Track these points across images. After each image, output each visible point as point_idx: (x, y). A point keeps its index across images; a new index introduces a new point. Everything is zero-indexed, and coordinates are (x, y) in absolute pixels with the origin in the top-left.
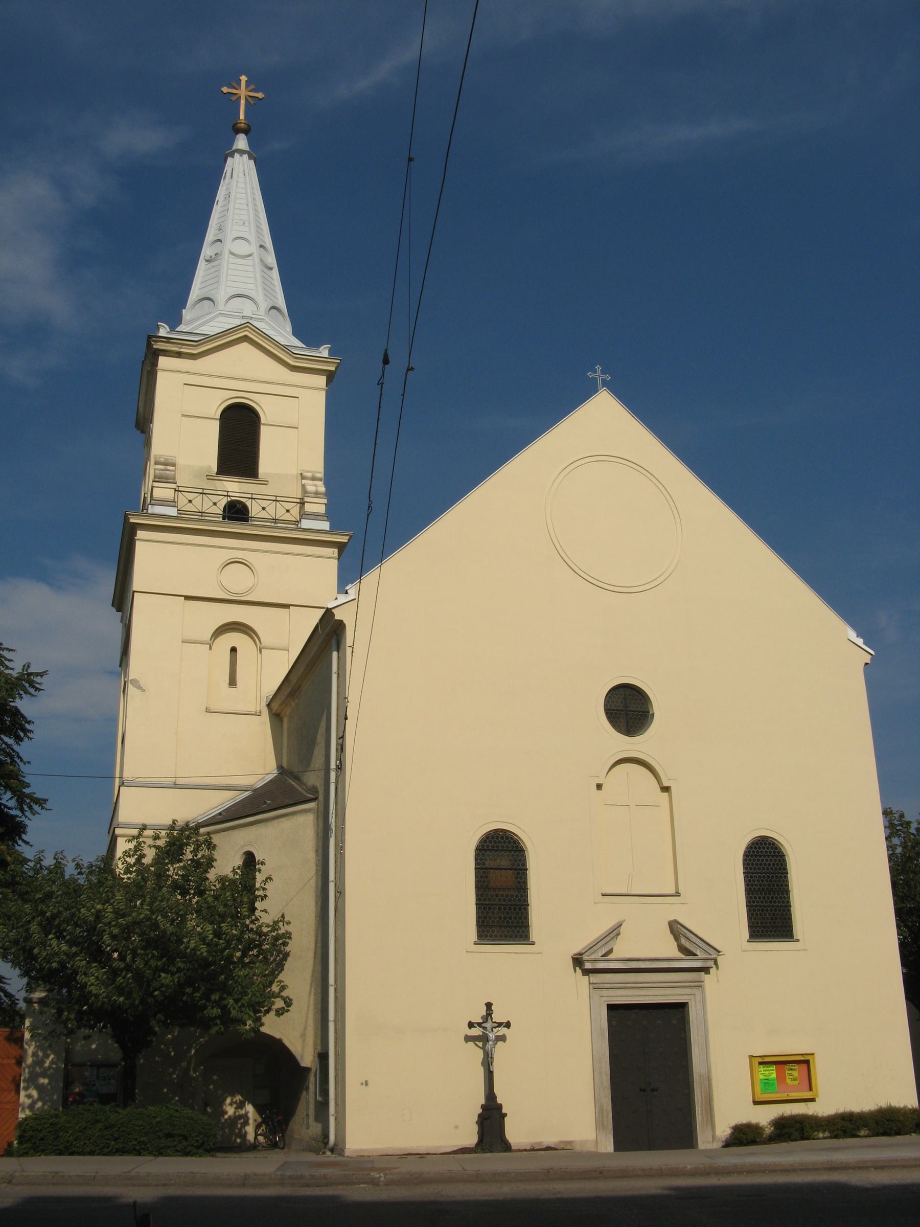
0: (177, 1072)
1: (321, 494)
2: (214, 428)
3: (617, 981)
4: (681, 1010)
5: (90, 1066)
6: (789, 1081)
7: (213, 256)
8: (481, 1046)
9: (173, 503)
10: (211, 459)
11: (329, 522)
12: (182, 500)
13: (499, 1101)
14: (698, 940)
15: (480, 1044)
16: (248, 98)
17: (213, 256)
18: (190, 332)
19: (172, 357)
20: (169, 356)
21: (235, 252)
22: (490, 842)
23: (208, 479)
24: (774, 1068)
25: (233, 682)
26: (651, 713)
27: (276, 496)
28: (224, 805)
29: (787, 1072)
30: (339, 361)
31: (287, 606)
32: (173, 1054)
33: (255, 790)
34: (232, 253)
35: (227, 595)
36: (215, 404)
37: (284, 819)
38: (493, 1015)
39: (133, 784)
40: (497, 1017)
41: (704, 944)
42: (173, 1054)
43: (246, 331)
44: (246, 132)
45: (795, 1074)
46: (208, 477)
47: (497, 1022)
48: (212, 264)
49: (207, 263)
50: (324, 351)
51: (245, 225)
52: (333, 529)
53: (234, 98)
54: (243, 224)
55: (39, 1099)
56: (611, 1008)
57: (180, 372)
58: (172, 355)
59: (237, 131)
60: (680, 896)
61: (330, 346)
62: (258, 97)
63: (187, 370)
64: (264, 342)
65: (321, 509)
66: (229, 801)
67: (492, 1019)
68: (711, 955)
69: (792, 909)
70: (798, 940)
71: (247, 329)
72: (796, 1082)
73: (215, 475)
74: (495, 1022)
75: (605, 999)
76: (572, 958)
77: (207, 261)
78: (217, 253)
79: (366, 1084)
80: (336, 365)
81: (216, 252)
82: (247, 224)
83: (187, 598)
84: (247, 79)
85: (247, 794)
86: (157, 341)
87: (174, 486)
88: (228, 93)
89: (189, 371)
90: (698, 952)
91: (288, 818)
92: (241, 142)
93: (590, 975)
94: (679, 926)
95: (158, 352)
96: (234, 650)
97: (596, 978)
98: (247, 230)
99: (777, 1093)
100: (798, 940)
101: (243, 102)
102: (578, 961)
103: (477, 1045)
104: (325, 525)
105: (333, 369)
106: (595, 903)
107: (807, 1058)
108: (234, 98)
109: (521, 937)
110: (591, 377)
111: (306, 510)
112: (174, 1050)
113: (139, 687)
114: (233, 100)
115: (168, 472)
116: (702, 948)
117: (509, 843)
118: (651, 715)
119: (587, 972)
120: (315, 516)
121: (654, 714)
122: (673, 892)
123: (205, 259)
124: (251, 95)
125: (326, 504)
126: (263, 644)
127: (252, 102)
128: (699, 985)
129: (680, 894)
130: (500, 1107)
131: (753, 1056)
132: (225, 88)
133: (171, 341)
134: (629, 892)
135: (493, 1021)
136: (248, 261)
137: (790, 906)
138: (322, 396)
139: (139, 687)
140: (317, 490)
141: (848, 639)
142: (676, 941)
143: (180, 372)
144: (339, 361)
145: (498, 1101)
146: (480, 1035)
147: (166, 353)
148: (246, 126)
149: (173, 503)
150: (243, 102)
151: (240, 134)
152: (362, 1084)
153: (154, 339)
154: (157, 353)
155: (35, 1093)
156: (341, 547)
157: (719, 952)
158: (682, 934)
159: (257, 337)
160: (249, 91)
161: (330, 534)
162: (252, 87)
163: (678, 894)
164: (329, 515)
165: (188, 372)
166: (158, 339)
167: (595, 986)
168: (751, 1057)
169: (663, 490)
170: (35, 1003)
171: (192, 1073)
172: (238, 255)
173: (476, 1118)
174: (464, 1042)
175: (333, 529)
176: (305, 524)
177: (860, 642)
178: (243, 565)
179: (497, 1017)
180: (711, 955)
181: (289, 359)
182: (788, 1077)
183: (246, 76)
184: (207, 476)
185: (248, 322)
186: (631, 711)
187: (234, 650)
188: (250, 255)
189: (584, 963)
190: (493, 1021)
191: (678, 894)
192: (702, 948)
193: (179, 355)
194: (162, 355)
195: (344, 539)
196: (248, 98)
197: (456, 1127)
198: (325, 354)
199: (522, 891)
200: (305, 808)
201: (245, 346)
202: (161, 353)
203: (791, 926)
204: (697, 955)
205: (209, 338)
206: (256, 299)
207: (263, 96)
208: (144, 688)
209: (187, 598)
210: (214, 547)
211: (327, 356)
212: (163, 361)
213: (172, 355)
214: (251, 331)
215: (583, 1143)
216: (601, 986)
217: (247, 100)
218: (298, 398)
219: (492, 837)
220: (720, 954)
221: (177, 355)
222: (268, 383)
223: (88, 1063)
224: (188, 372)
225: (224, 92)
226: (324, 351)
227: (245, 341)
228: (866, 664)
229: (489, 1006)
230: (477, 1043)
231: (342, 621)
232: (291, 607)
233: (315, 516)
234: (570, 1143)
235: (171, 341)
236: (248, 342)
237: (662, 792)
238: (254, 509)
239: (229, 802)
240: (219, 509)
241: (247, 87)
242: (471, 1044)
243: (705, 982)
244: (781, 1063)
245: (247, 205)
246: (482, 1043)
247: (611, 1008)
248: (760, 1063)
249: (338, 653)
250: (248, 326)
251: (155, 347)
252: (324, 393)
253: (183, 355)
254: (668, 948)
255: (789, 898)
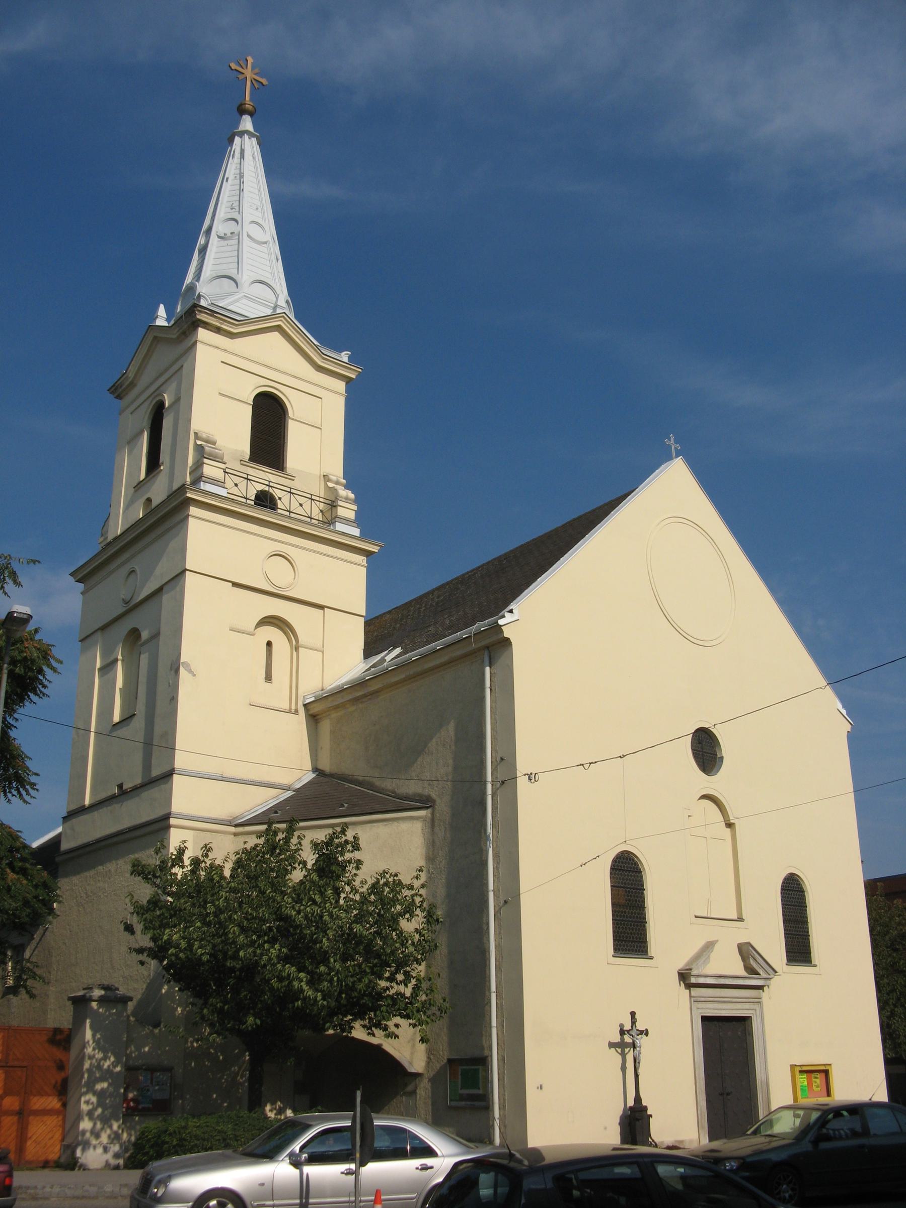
0: (225, 1077)
1: (350, 500)
2: (249, 411)
3: (710, 995)
4: (743, 1023)
5: (145, 1070)
6: (814, 1088)
7: (229, 235)
8: (620, 1052)
9: (221, 484)
10: (243, 445)
11: (359, 530)
12: (229, 483)
13: (644, 1103)
14: (763, 961)
15: (619, 1050)
16: (253, 81)
17: (229, 235)
18: (225, 307)
19: (211, 331)
20: (208, 329)
21: (252, 236)
22: (619, 862)
23: (242, 464)
24: (806, 1076)
25: (268, 678)
26: (718, 756)
27: (311, 495)
28: (268, 802)
29: (813, 1080)
30: (360, 370)
31: (321, 607)
32: (221, 1058)
33: (297, 790)
34: (248, 236)
35: (274, 589)
36: (249, 390)
37: (380, 824)
38: (636, 1023)
39: (183, 774)
40: (640, 1026)
41: (765, 964)
42: (221, 1058)
43: (281, 320)
44: (251, 114)
45: (818, 1081)
46: (242, 462)
47: (639, 1029)
48: (226, 242)
49: (220, 240)
50: (345, 356)
51: (258, 210)
52: (364, 537)
53: (241, 77)
54: (257, 209)
55: (99, 1104)
56: (705, 1019)
57: (218, 348)
58: (212, 329)
59: (242, 111)
60: (743, 921)
61: (350, 353)
62: (262, 83)
63: (225, 348)
64: (295, 335)
65: (351, 515)
66: (272, 799)
67: (636, 1027)
68: (769, 975)
69: (810, 938)
70: (815, 966)
71: (282, 319)
72: (819, 1089)
73: (247, 461)
74: (632, 1027)
75: (700, 1011)
76: (678, 973)
77: (219, 237)
78: (234, 233)
79: (541, 1088)
80: (357, 374)
81: (233, 231)
82: (260, 209)
83: (235, 584)
84: (253, 61)
85: (289, 794)
86: (201, 312)
87: (223, 466)
88: (235, 70)
89: (227, 349)
90: (761, 972)
91: (385, 823)
92: (247, 123)
93: (691, 988)
94: (750, 948)
95: (199, 323)
96: (269, 644)
97: (696, 992)
98: (260, 215)
99: (808, 1098)
100: (815, 966)
101: (249, 83)
102: (684, 976)
103: (617, 1051)
104: (356, 532)
105: (354, 377)
106: (691, 924)
107: (827, 1068)
108: (241, 77)
109: (642, 951)
110: (667, 443)
111: (338, 514)
112: (222, 1054)
113: (190, 671)
114: (240, 79)
115: (217, 451)
116: (764, 969)
117: (632, 864)
118: (719, 758)
119: (689, 986)
120: (346, 521)
121: (722, 757)
122: (735, 917)
123: (217, 235)
124: (256, 78)
125: (355, 511)
126: (301, 642)
127: (256, 86)
128: (758, 1002)
129: (743, 919)
130: (646, 1108)
131: (795, 1065)
132: (233, 64)
133: (215, 315)
134: (709, 916)
135: (637, 1028)
136: (263, 248)
137: (809, 936)
138: (341, 401)
139: (190, 671)
140: (347, 495)
141: (838, 709)
142: (743, 961)
143: (218, 348)
144: (360, 370)
145: (643, 1103)
146: (619, 1042)
147: (206, 325)
148: (253, 109)
149: (221, 484)
150: (249, 83)
151: (247, 116)
152: (538, 1088)
153: (200, 309)
154: (197, 324)
155: (94, 1099)
156: (368, 554)
157: (776, 972)
158: (752, 956)
159: (290, 329)
160: (254, 74)
161: (358, 540)
162: (257, 70)
163: (740, 919)
164: (359, 521)
165: (225, 350)
166: (203, 310)
167: (695, 999)
168: (793, 1067)
169: (721, 556)
170: (94, 1001)
171: (239, 1078)
172: (254, 239)
173: (618, 1121)
174: (608, 1048)
175: (364, 537)
176: (340, 527)
177: (844, 712)
178: (284, 559)
179: (640, 1026)
180: (769, 975)
181: (318, 359)
182: (814, 1084)
183: (253, 58)
184: (241, 460)
185: (284, 313)
186: (706, 753)
187: (269, 644)
188: (265, 243)
189: (690, 977)
190: (637, 1028)
191: (740, 919)
192: (764, 969)
193: (218, 330)
194: (201, 327)
195: (375, 549)
196: (253, 81)
197: (605, 1128)
198: (346, 359)
199: (641, 909)
200: (411, 815)
201: (276, 335)
202: (202, 325)
203: (809, 953)
204: (759, 974)
205: (248, 321)
206: (276, 289)
207: (267, 83)
208: (195, 673)
209: (235, 584)
210: (261, 537)
211: (347, 362)
212: (202, 333)
213: (212, 329)
214: (285, 322)
215: (691, 1141)
216: (699, 999)
217: (253, 83)
218: (321, 398)
219: (620, 858)
220: (777, 974)
221: (217, 331)
222: (296, 377)
223: (144, 1067)
224: (225, 350)
225: (233, 68)
226: (345, 356)
227: (277, 331)
228: (848, 732)
229: (633, 1014)
230: (617, 1049)
231: (509, 639)
232: (325, 609)
233: (346, 521)
234: (682, 1142)
235: (215, 315)
236: (279, 332)
237: (727, 827)
238: (284, 501)
239: (272, 801)
240: (252, 494)
241: (253, 68)
242: (613, 1049)
243: (763, 999)
244: (809, 1072)
245: (259, 191)
246: (620, 1049)
247: (705, 1019)
248: (801, 1072)
249: (490, 668)
250: (283, 317)
251: (198, 317)
252: (343, 399)
253: (222, 332)
254: (736, 968)
255: (808, 928)
